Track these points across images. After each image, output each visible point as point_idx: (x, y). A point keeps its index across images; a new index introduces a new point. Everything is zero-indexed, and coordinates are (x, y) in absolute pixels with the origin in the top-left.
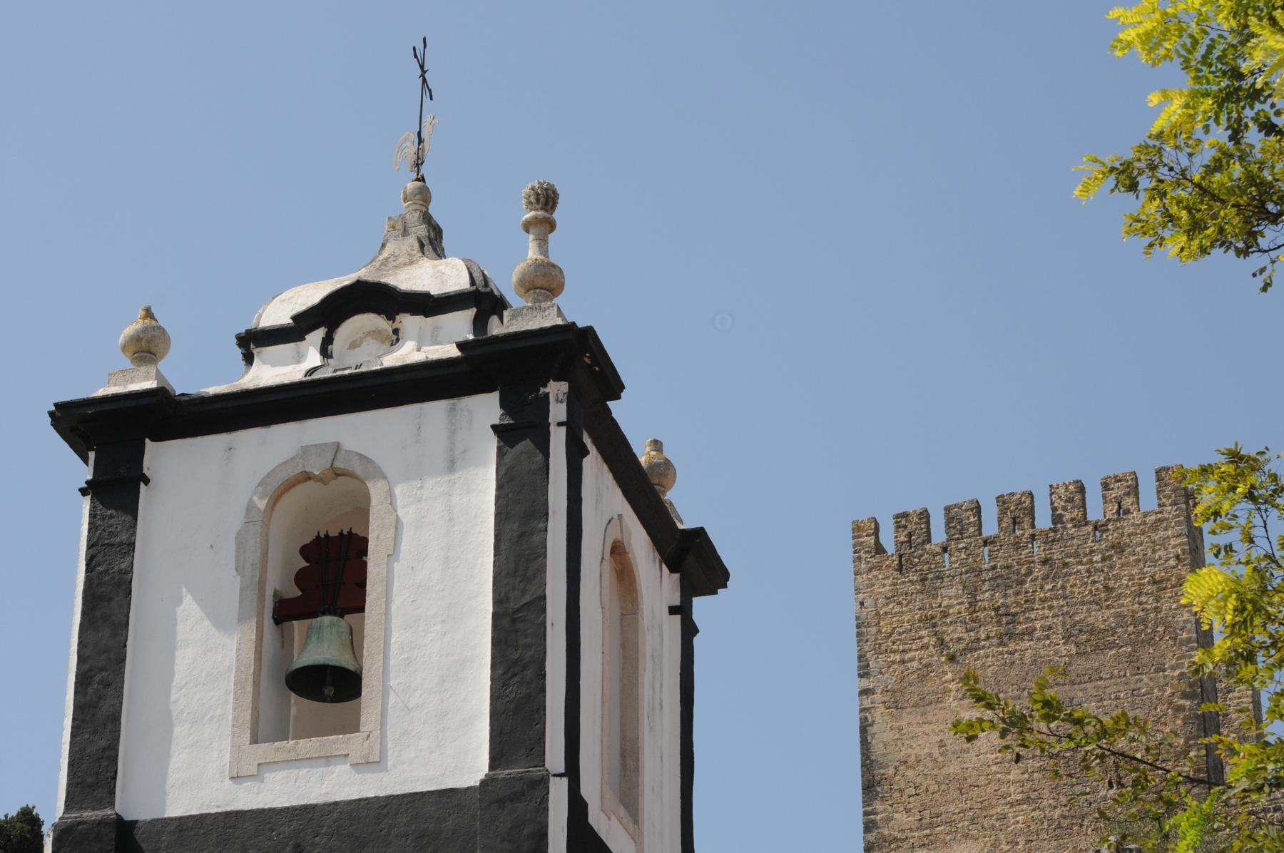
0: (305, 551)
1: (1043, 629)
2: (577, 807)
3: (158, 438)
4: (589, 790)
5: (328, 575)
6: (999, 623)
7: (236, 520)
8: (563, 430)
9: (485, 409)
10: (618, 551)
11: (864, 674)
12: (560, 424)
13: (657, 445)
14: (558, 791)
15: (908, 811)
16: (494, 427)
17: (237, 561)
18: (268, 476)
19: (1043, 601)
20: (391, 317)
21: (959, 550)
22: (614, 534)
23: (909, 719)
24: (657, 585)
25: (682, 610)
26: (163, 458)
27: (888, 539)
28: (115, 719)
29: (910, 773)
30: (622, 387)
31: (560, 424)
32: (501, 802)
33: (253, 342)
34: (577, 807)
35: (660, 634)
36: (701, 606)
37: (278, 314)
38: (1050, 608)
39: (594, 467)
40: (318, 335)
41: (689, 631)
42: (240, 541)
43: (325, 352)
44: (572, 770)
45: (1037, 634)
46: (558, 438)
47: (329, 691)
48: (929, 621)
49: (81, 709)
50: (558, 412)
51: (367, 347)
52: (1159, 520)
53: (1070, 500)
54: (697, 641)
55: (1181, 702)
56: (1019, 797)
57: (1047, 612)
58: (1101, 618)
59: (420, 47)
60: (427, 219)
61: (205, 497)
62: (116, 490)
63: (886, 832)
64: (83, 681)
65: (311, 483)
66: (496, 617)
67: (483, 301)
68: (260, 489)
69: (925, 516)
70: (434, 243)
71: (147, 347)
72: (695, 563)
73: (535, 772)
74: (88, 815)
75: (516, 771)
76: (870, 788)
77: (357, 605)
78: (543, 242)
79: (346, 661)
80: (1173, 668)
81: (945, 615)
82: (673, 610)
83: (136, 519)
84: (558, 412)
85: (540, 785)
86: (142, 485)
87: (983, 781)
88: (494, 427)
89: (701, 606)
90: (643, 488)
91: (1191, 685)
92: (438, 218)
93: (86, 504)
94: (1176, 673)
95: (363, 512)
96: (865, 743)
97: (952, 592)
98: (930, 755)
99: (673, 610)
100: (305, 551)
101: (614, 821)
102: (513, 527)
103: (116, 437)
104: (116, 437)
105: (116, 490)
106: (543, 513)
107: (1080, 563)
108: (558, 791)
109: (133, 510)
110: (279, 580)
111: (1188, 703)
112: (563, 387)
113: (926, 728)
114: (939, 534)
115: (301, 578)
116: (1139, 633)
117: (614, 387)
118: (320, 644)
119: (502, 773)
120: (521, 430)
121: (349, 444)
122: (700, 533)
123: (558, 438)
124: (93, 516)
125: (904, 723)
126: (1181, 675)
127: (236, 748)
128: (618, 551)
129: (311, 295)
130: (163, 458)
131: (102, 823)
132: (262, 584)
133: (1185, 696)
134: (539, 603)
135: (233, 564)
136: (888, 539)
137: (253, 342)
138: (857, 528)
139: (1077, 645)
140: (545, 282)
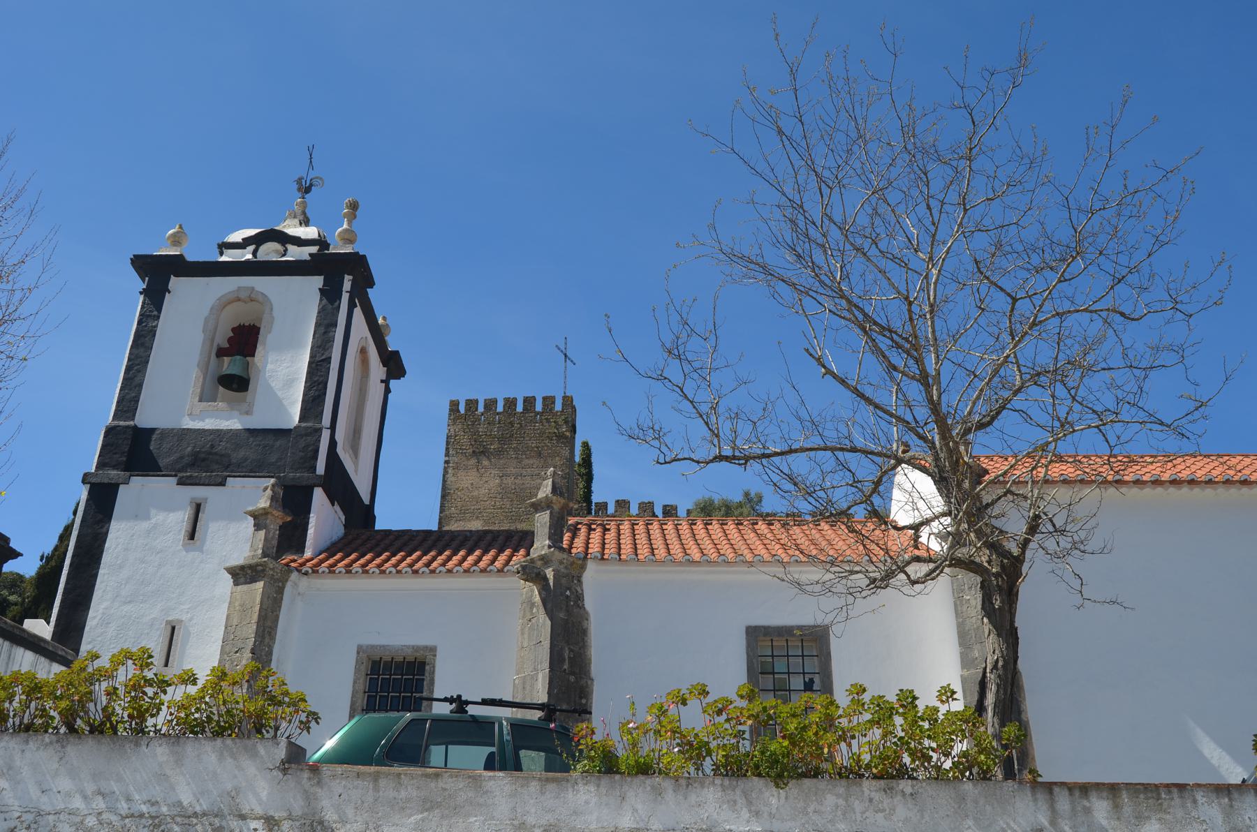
0: (233, 330)
2: (333, 444)
4: (340, 436)
5: (244, 340)
7: (206, 312)
9: (318, 281)
10: (363, 351)
11: (447, 455)
13: (384, 318)
14: (326, 435)
20: (283, 245)
22: (363, 344)
23: (461, 473)
24: (377, 370)
25: (386, 382)
26: (175, 283)
27: (462, 409)
28: (141, 385)
32: (302, 436)
33: (224, 246)
34: (333, 444)
35: (376, 390)
36: (393, 383)
37: (237, 237)
39: (358, 312)
40: (251, 248)
41: (387, 391)
42: (207, 320)
43: (255, 253)
44: (333, 427)
46: (345, 298)
47: (235, 386)
49: (127, 380)
50: (347, 285)
51: (270, 251)
60: (304, 213)
61: (191, 303)
62: (155, 296)
64: (128, 369)
66: (310, 363)
67: (321, 243)
69: (477, 401)
70: (306, 222)
71: (176, 240)
72: (394, 366)
73: (318, 426)
74: (122, 423)
75: (310, 424)
76: (443, 497)
77: (252, 354)
78: (350, 223)
82: (382, 381)
83: (160, 311)
84: (347, 285)
85: (318, 431)
89: (393, 383)
90: (378, 333)
92: (309, 215)
93: (141, 298)
95: (261, 320)
96: (444, 481)
99: (382, 381)
100: (233, 330)
102: (322, 330)
103: (158, 273)
104: (158, 273)
105: (155, 296)
106: (334, 325)
108: (326, 435)
109: (153, 430)
110: (222, 340)
114: (481, 409)
115: (230, 340)
117: (371, 284)
119: (303, 425)
120: (330, 294)
121: (258, 288)
123: (345, 298)
124: (144, 303)
128: (363, 351)
129: (252, 232)
130: (175, 283)
131: (128, 427)
132: (212, 341)
134: (328, 360)
136: (462, 409)
137: (224, 246)
138: (452, 402)
140: (349, 238)
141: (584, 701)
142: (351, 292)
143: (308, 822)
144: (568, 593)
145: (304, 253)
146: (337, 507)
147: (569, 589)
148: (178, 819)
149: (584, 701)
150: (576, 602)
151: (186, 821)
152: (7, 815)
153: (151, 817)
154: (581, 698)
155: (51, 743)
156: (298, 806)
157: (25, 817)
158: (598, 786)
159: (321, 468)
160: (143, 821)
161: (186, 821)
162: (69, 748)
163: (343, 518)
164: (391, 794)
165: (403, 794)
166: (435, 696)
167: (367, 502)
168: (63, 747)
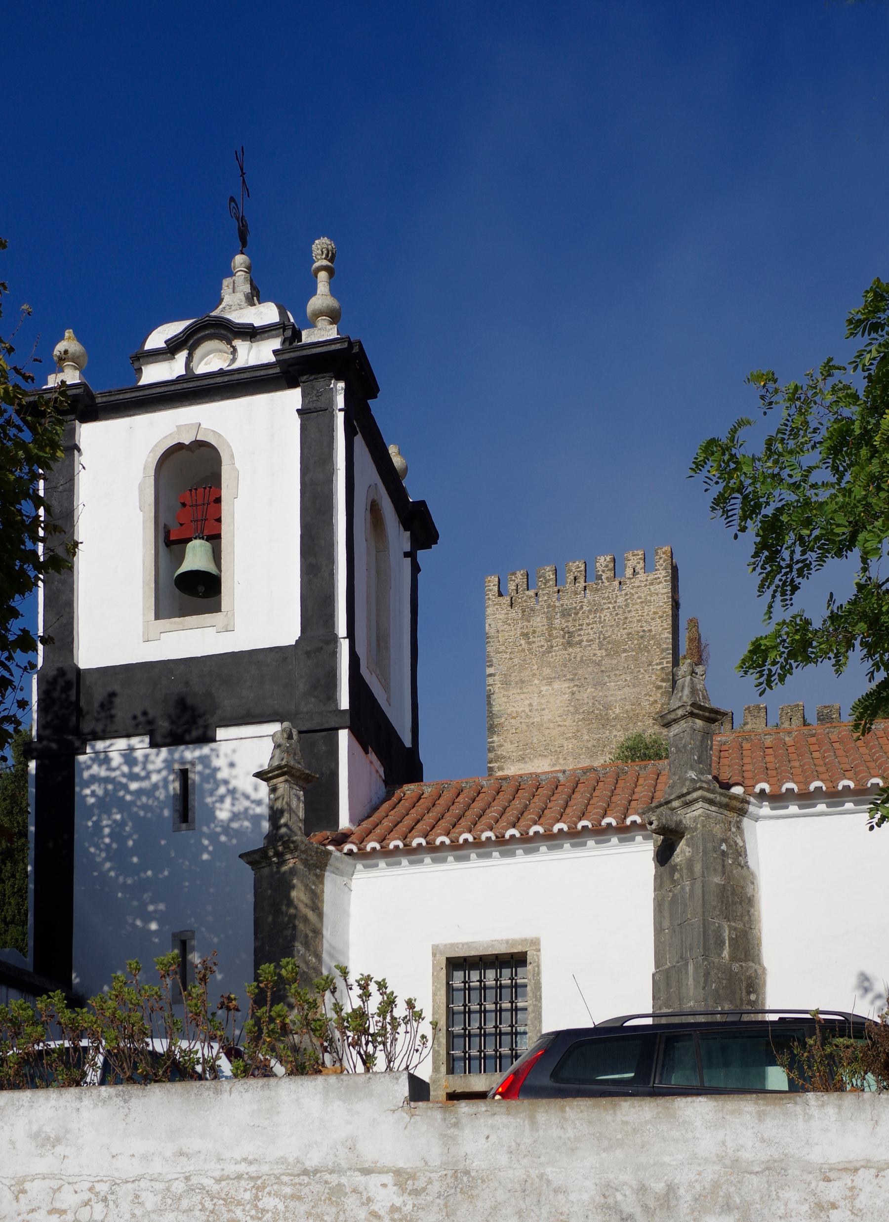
1: (588, 641)
3: (84, 420)
6: (564, 637)
8: (342, 413)
12: (340, 410)
15: (511, 742)
16: (298, 410)
17: (140, 503)
18: (156, 446)
19: (588, 624)
20: (229, 342)
21: (544, 595)
24: (399, 539)
29: (513, 721)
30: (378, 390)
31: (340, 410)
36: (421, 554)
38: (592, 628)
39: (358, 440)
41: (416, 569)
45: (584, 643)
48: (525, 635)
52: (656, 579)
53: (607, 566)
54: (420, 576)
55: (660, 684)
56: (570, 735)
57: (590, 631)
58: (620, 634)
59: (239, 153)
63: (499, 753)
65: (184, 451)
68: (151, 454)
79: (210, 567)
80: (657, 664)
81: (534, 632)
82: (406, 555)
84: (340, 401)
86: (76, 452)
87: (551, 725)
88: (298, 410)
91: (667, 674)
94: (659, 667)
97: (539, 619)
98: (524, 711)
99: (406, 555)
101: (374, 676)
107: (610, 603)
111: (664, 684)
112: (341, 385)
113: (522, 696)
116: (640, 644)
118: (196, 557)
122: (423, 503)
125: (510, 693)
126: (663, 668)
127: (146, 622)
128: (374, 509)
129: (174, 329)
133: (663, 680)
135: (138, 504)
139: (606, 650)
141: (753, 997)
142: (347, 410)
143: (450, 1173)
144: (724, 847)
145: (263, 353)
146: (373, 757)
147: (724, 840)
148: (285, 1179)
149: (753, 997)
150: (735, 860)
151: (297, 1180)
152: (76, 1187)
153: (251, 1178)
154: (749, 993)
155: (110, 1097)
156: (435, 1154)
157: (99, 1187)
158: (840, 1107)
159: (344, 703)
160: (243, 1183)
161: (297, 1180)
162: (134, 1102)
163: (381, 771)
164: (556, 1132)
165: (571, 1133)
166: (767, 1008)
167: (408, 744)
168: (125, 1101)
